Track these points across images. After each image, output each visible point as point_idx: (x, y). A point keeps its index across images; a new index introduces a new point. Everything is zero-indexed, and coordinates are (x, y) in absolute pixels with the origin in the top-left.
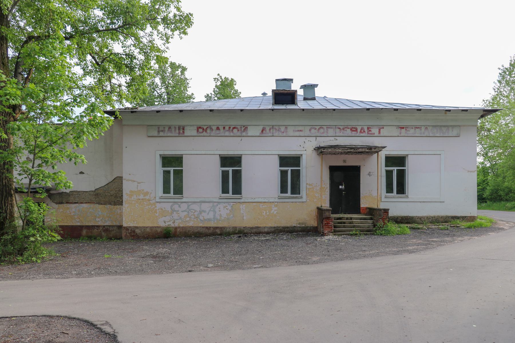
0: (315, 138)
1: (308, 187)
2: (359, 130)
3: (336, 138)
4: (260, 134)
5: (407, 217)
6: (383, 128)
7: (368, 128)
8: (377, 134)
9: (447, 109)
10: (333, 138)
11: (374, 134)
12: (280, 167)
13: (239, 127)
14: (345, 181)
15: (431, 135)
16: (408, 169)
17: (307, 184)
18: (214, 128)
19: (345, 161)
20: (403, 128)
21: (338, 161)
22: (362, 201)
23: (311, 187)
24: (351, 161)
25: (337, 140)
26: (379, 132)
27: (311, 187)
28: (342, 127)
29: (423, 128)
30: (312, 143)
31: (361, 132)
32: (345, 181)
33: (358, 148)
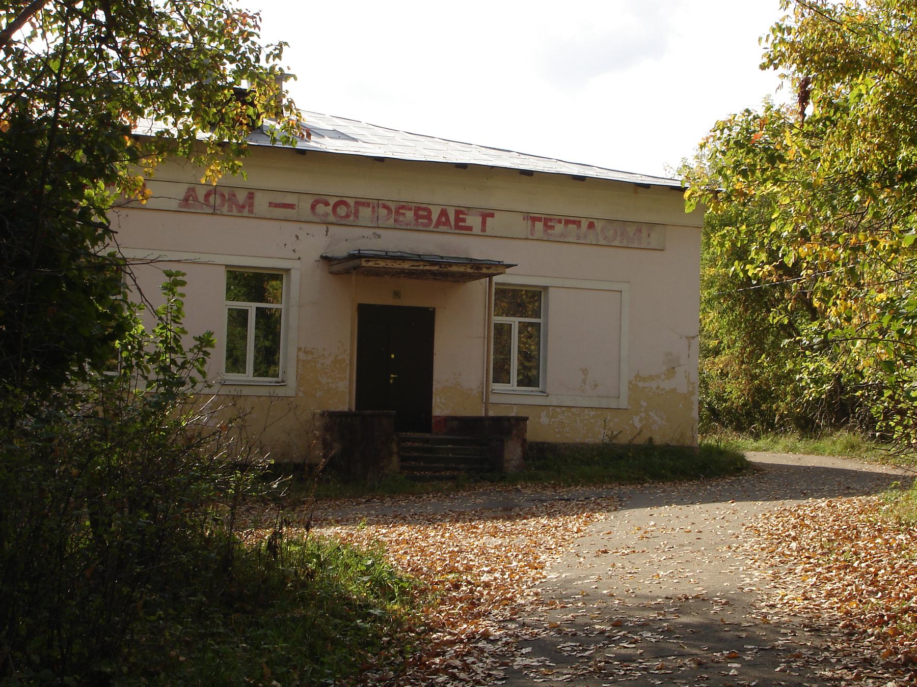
0: (324, 227)
1: (302, 356)
2: (435, 217)
3: (378, 231)
4: (180, 206)
5: (543, 443)
6: (492, 215)
7: (458, 213)
8: (477, 229)
9: (639, 180)
10: (368, 232)
11: (470, 228)
12: (228, 298)
13: (351, 202)
14: (394, 342)
15: (602, 242)
16: (546, 324)
17: (299, 349)
18: (585, 224)
19: (397, 294)
20: (539, 219)
21: (380, 296)
22: (437, 400)
23: (310, 357)
24: (414, 297)
25: (379, 236)
26: (483, 230)
27: (310, 357)
28: (393, 206)
29: (631, 230)
30: (315, 241)
31: (439, 223)
32: (394, 342)
33: (450, 264)
